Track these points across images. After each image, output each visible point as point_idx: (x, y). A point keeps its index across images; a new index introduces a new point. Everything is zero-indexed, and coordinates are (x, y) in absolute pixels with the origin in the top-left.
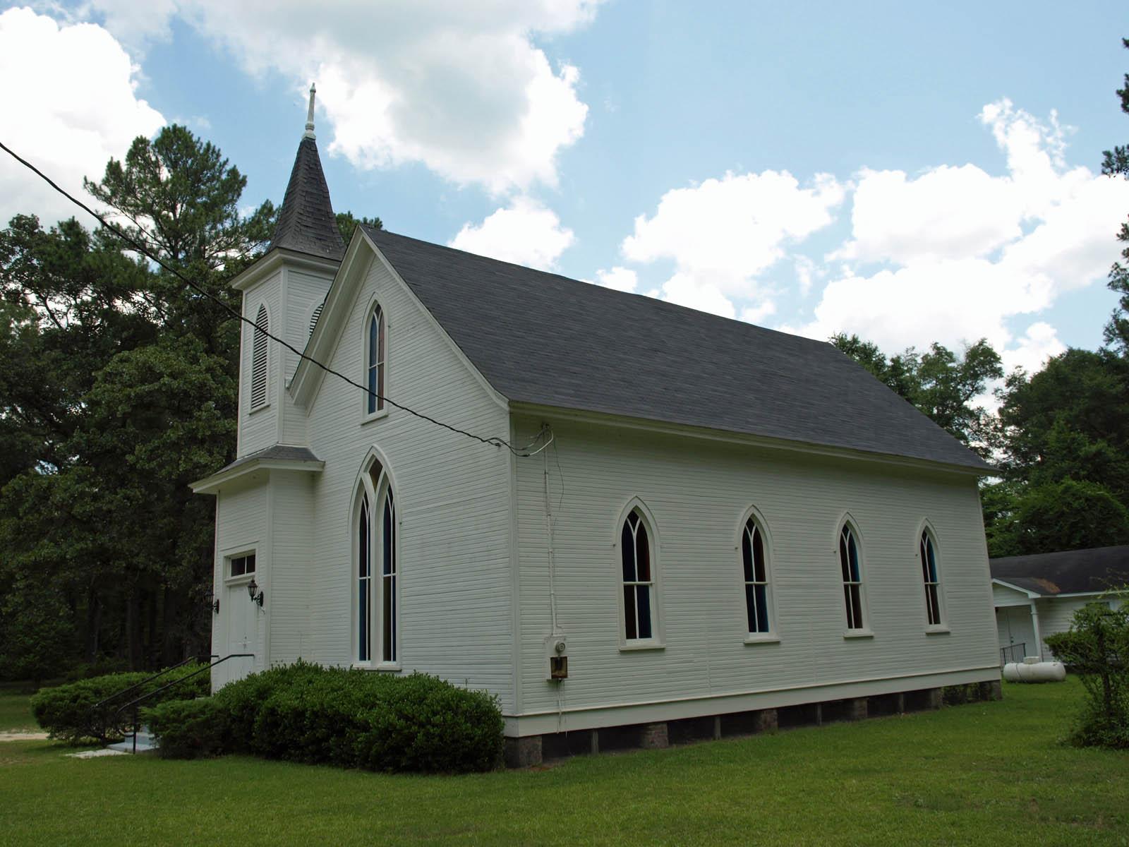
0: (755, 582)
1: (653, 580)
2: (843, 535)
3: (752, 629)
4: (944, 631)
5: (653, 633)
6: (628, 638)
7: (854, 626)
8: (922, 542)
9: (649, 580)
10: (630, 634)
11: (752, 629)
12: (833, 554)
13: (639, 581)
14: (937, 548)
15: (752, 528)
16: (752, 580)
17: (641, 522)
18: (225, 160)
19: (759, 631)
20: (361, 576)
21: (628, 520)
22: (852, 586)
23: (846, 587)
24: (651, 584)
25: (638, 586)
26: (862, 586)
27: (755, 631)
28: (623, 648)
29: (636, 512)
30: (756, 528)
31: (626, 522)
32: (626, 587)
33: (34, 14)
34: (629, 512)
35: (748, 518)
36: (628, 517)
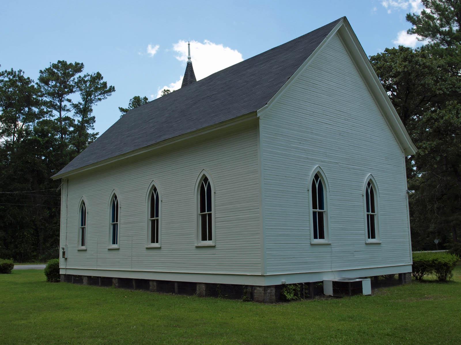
0: (318, 210)
3: (315, 237)
5: (376, 238)
6: (314, 238)
7: (155, 242)
8: (367, 188)
11: (315, 237)
14: (376, 194)
15: (318, 180)
19: (372, 238)
20: (367, 212)
21: (314, 178)
22: (371, 215)
23: (314, 213)
24: (375, 214)
28: (149, 246)
30: (320, 180)
31: (314, 179)
33: (346, 17)
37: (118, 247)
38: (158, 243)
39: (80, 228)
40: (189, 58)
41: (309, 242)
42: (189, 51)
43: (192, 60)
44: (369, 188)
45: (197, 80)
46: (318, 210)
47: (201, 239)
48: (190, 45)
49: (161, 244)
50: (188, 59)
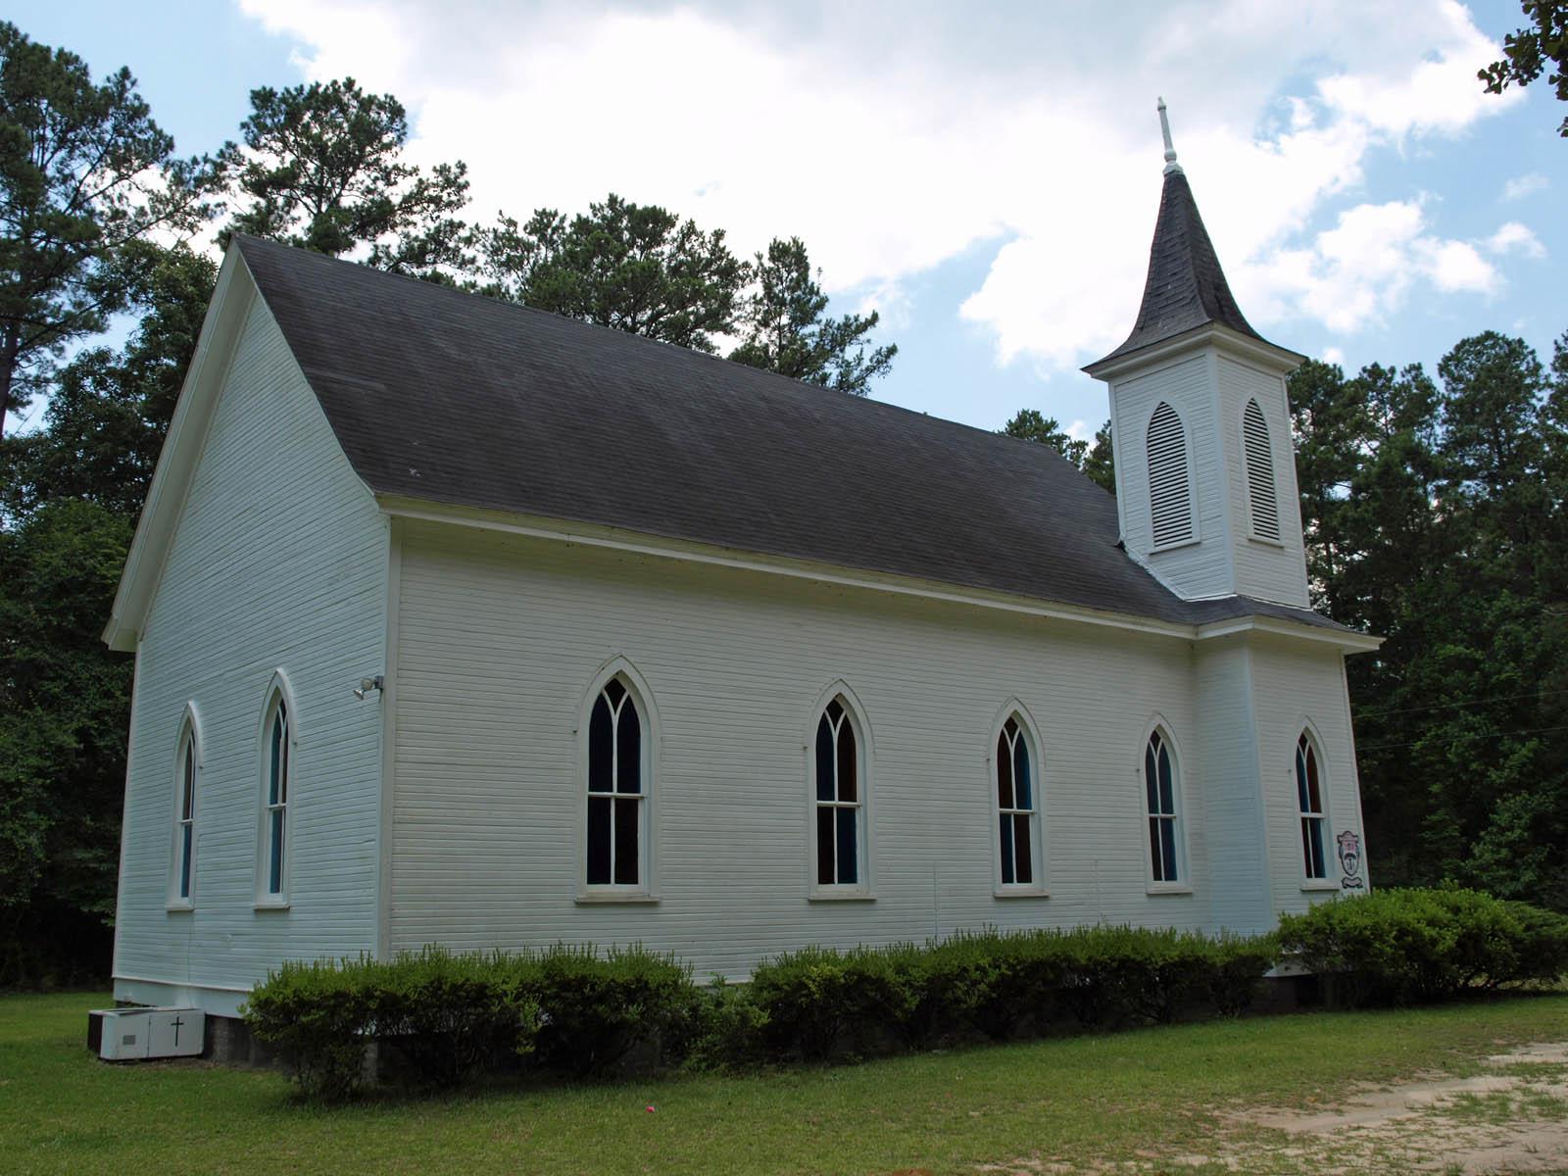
1: (644, 790)
2: (1152, 745)
3: (1007, 878)
4: (832, 898)
5: (859, 877)
6: (1004, 882)
7: (1163, 878)
9: (638, 791)
10: (825, 877)
12: (1135, 773)
13: (840, 800)
16: (1012, 807)
17: (846, 716)
18: (865, 315)
20: (1150, 812)
21: (827, 714)
24: (642, 798)
25: (840, 809)
26: (1178, 820)
27: (1160, 879)
29: (1014, 719)
31: (824, 715)
32: (1151, 819)
34: (830, 700)
35: (1007, 717)
36: (827, 708)
37: (285, 903)
38: (187, 896)
39: (267, 812)
40: (1170, 157)
41: (991, 892)
42: (1162, 123)
43: (1180, 161)
44: (1156, 750)
45: (7, 412)
46: (836, 802)
47: (606, 885)
48: (1165, 108)
49: (194, 899)
50: (1167, 161)
